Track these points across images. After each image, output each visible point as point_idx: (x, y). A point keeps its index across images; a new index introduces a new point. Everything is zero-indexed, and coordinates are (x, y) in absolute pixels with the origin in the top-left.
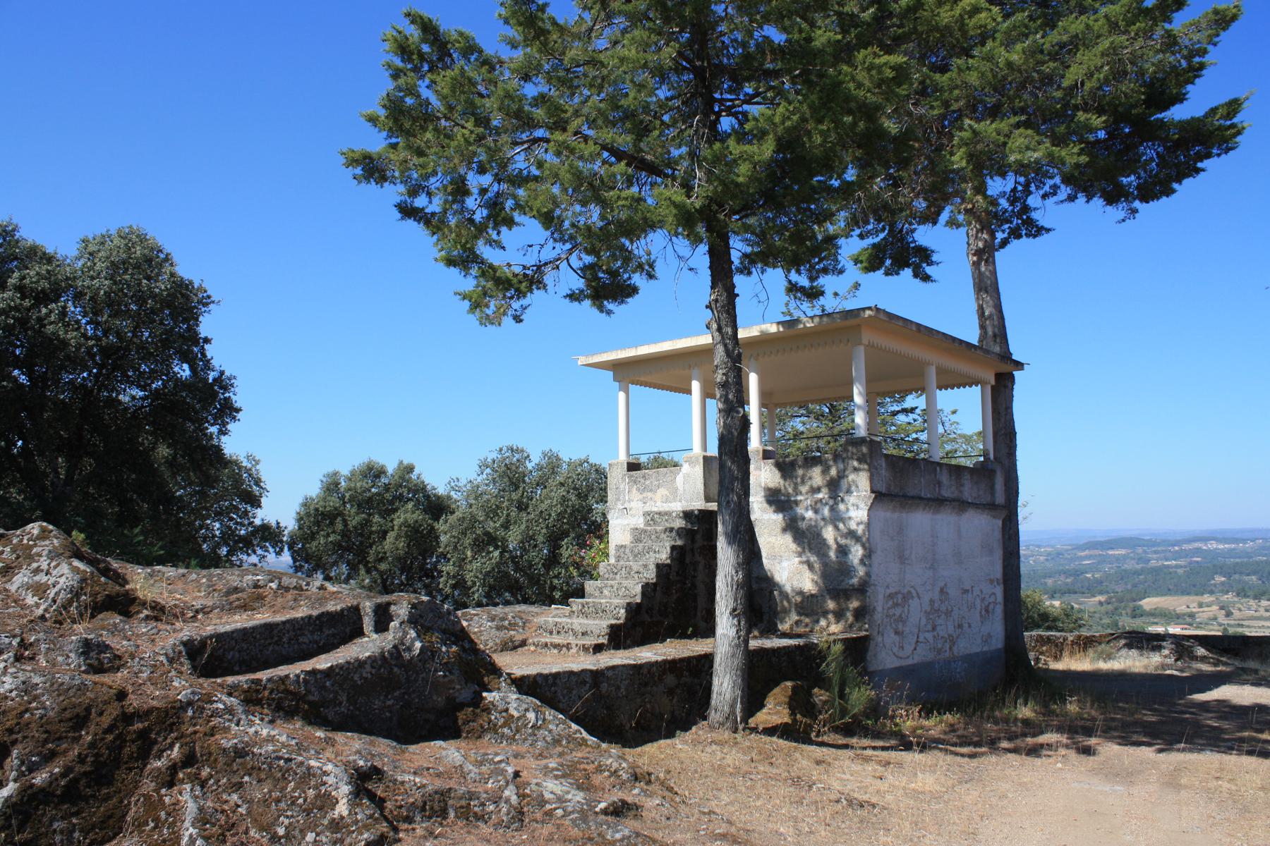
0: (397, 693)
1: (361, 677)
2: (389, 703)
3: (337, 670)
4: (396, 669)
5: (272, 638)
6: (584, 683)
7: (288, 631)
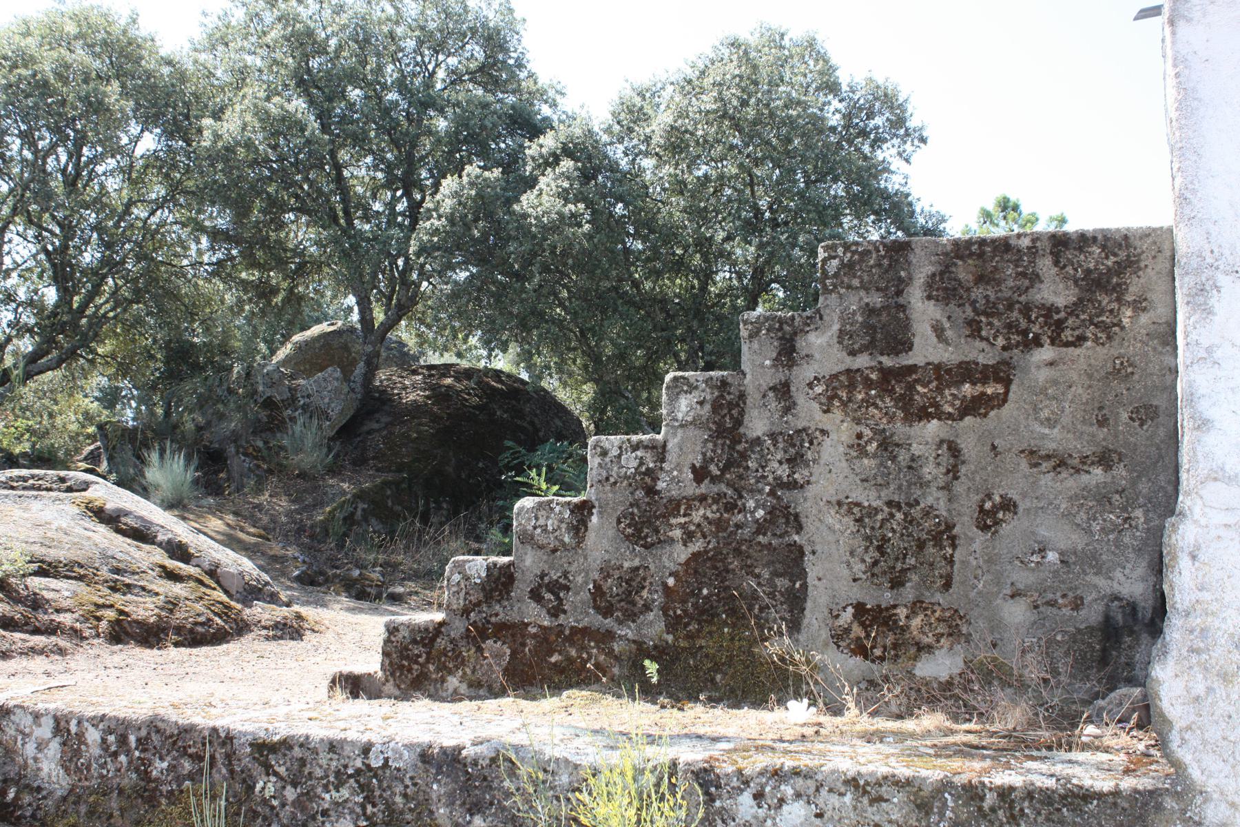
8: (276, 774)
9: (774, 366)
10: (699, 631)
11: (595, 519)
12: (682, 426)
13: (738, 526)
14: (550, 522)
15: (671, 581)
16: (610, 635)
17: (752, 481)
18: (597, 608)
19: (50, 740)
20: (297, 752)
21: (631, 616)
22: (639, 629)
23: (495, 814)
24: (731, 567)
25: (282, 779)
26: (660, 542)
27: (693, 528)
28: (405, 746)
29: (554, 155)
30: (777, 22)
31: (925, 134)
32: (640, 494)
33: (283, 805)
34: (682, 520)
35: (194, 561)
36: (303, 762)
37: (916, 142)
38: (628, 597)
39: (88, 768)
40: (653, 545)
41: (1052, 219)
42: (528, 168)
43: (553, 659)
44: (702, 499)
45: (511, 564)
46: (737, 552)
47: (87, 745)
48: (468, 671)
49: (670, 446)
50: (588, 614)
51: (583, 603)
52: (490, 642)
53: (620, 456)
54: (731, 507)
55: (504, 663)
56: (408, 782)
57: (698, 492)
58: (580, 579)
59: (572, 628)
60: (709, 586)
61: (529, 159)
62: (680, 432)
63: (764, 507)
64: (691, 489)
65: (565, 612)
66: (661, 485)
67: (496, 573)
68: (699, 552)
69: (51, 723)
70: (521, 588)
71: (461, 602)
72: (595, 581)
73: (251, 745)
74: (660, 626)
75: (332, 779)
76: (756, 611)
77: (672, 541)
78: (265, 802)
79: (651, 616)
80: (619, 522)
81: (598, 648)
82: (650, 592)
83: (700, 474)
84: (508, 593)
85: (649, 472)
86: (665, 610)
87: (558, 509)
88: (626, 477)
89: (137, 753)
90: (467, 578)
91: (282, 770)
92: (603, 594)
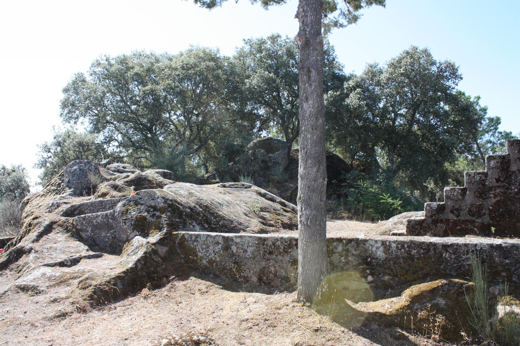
0: (112, 231)
1: (97, 222)
2: (108, 235)
3: (87, 218)
4: (110, 220)
5: (102, 206)
6: (218, 243)
7: (109, 204)
8: (449, 252)
9: (518, 153)
10: (500, 220)
11: (468, 192)
12: (492, 168)
13: (510, 193)
14: (455, 193)
15: (491, 208)
16: (474, 221)
17: (513, 182)
18: (470, 215)
19: (380, 247)
20: (455, 247)
21: (480, 216)
22: (482, 220)
23: (512, 259)
24: (508, 204)
25: (451, 253)
26: (487, 198)
27: (496, 194)
28: (486, 244)
29: (353, 87)
30: (416, 45)
31: (462, 77)
32: (480, 186)
33: (451, 259)
34: (493, 192)
35: (288, 207)
36: (457, 249)
37: (459, 79)
38: (479, 212)
39: (392, 253)
40: (485, 199)
41: (475, 97)
42: (345, 91)
43: (458, 228)
44: (499, 187)
45: (444, 204)
46: (510, 200)
47: (392, 248)
48: (433, 231)
49: (489, 173)
50: (467, 216)
51: (465, 213)
52: (439, 224)
53: (474, 176)
54: (507, 189)
55: (443, 229)
56: (487, 252)
57: (497, 185)
58: (464, 208)
59: (463, 220)
60: (502, 209)
61: (345, 89)
62: (491, 170)
63: (517, 188)
64: (496, 184)
65: (460, 216)
66: (487, 183)
67: (440, 206)
68: (498, 200)
69: (381, 243)
70: (447, 210)
71: (430, 214)
72: (469, 208)
73: (442, 246)
74: (488, 219)
75: (465, 253)
76: (516, 215)
77: (490, 197)
78: (446, 259)
79: (486, 216)
80: (475, 193)
81: (471, 224)
82: (485, 210)
83: (498, 180)
84: (444, 211)
85: (483, 180)
86: (489, 215)
87: (457, 190)
88: (476, 181)
89: (407, 249)
90: (431, 208)
91: (451, 251)
92: (471, 211)
